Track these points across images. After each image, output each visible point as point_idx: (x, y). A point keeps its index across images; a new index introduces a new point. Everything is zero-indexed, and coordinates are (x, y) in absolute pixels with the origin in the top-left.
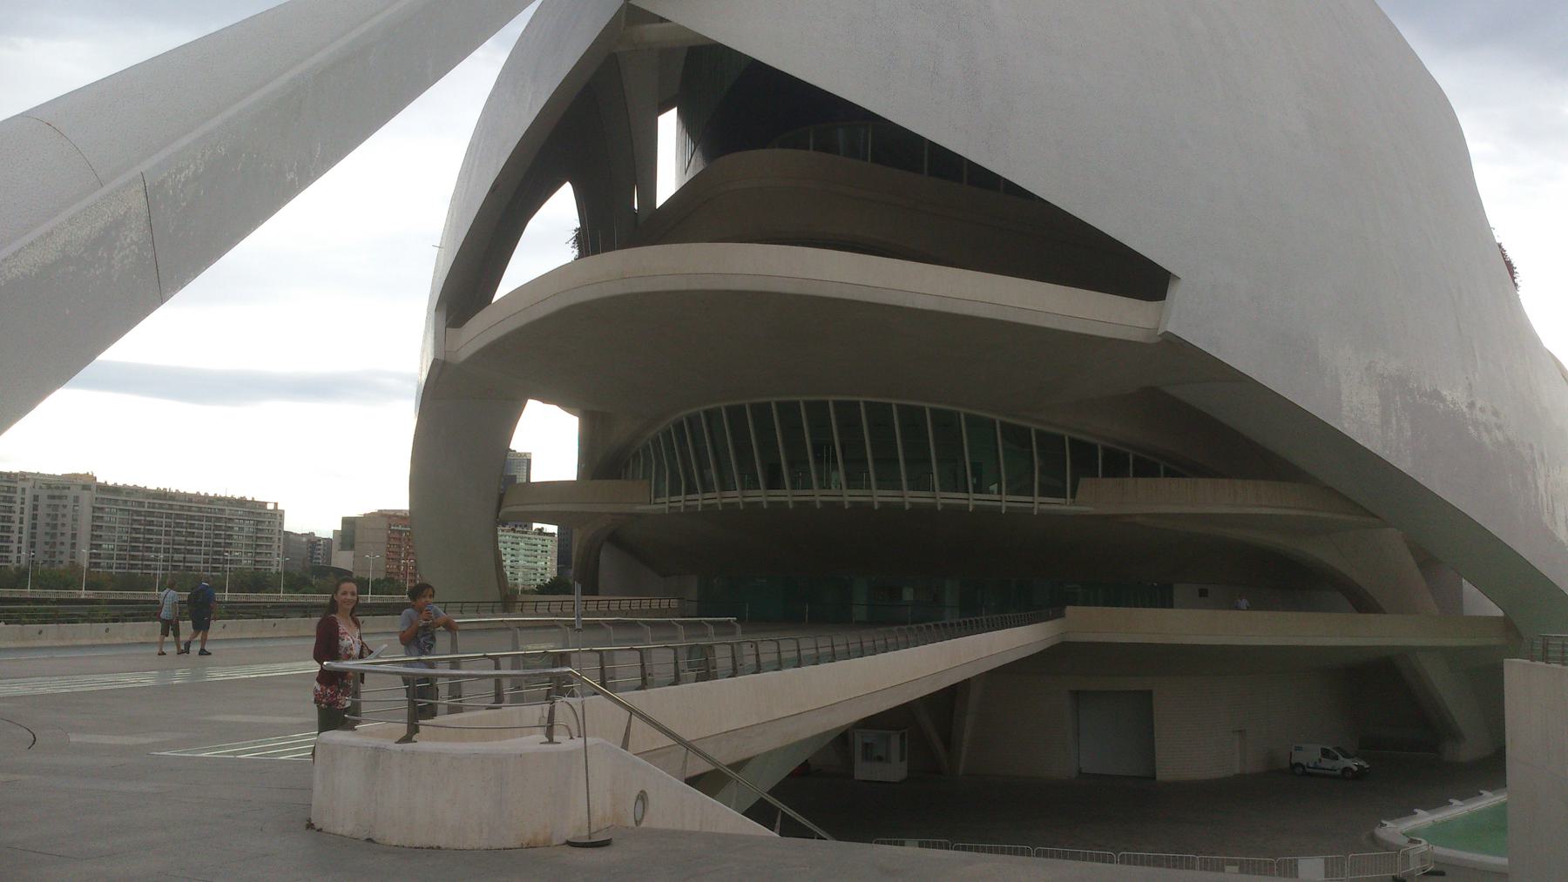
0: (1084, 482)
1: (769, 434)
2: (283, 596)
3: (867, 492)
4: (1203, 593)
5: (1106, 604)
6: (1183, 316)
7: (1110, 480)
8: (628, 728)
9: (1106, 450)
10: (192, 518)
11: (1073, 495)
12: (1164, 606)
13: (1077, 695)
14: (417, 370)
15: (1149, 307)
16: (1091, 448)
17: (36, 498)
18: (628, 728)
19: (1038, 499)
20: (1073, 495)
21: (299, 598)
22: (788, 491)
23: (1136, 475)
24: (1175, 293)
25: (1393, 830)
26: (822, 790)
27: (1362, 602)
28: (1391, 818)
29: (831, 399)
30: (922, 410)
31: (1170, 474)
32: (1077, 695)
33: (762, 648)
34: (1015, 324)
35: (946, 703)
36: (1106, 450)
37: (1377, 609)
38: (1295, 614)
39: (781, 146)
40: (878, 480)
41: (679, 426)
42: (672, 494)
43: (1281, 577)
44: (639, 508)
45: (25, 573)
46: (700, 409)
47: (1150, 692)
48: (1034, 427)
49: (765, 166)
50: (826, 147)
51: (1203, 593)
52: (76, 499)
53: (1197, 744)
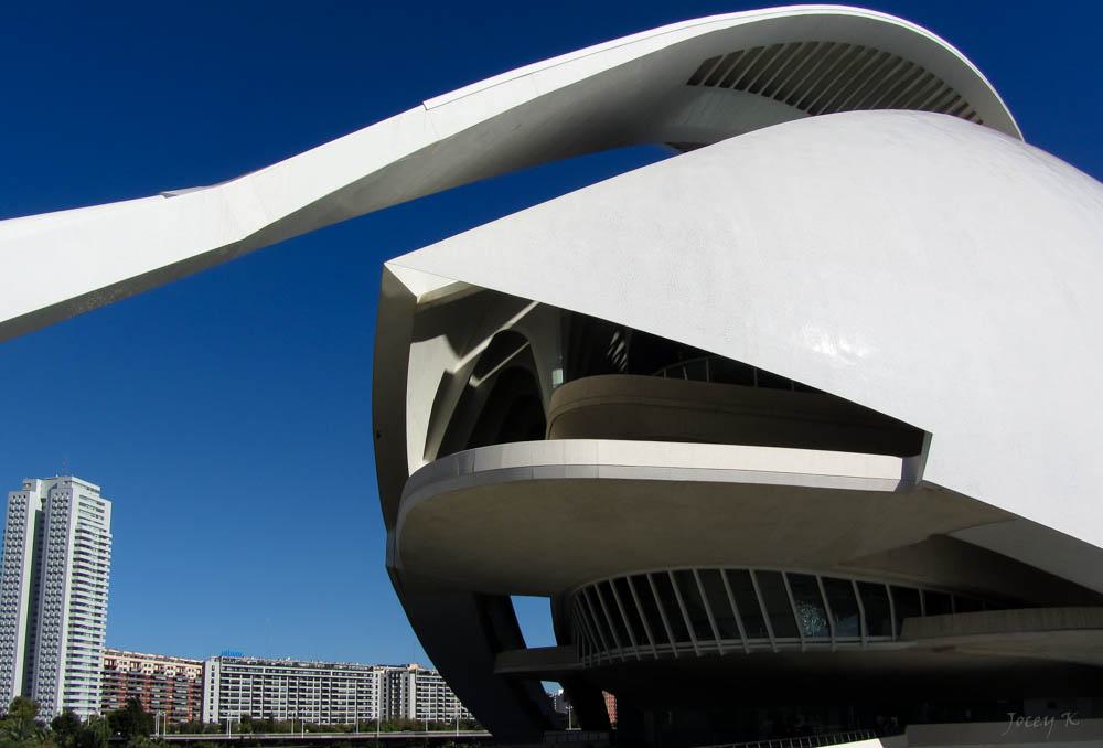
0: (909, 622)
3: (764, 640)
7: (930, 618)
9: (928, 594)
11: (899, 633)
16: (914, 592)
22: (744, 639)
23: (959, 610)
30: (849, 583)
48: (854, 579)
51: (1052, 706)
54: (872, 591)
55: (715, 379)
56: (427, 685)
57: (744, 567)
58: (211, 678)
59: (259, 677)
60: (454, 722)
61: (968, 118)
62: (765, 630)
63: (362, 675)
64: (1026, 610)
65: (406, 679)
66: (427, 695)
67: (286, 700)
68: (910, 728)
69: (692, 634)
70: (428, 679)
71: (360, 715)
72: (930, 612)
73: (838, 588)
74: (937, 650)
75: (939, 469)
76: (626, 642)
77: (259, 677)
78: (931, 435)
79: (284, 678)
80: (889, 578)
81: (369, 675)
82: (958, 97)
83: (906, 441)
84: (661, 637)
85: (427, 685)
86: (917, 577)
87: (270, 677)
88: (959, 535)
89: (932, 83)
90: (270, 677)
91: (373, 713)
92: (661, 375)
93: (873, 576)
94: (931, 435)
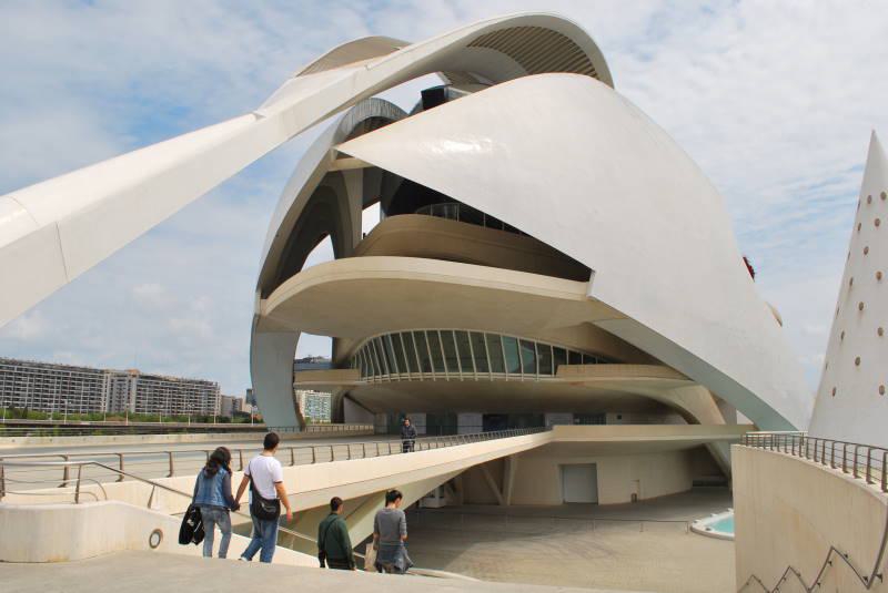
1: (403, 347)
2: (215, 425)
4: (619, 417)
6: (598, 288)
8: (314, 124)
9: (571, 353)
13: (563, 467)
15: (583, 284)
16: (563, 351)
17: (112, 381)
18: (314, 124)
19: (539, 375)
22: (433, 373)
23: (585, 363)
24: (595, 279)
25: (701, 524)
27: (690, 420)
29: (469, 330)
30: (466, 333)
31: (601, 362)
32: (563, 467)
35: (500, 465)
36: (585, 356)
37: (699, 423)
40: (463, 367)
41: (370, 343)
43: (653, 410)
46: (380, 335)
47: (594, 465)
48: (536, 341)
49: (409, 222)
50: (440, 214)
51: (619, 417)
53: (614, 488)
55: (462, 219)
57: (479, 331)
59: (11, 374)
61: (594, 76)
64: (612, 365)
66: (79, 398)
67: (59, 395)
69: (475, 369)
72: (571, 363)
75: (600, 288)
76: (403, 370)
77: (11, 374)
78: (424, 93)
79: (31, 376)
82: (590, 65)
84: (403, 370)
86: (569, 343)
87: (20, 374)
88: (602, 325)
90: (20, 374)
92: (427, 213)
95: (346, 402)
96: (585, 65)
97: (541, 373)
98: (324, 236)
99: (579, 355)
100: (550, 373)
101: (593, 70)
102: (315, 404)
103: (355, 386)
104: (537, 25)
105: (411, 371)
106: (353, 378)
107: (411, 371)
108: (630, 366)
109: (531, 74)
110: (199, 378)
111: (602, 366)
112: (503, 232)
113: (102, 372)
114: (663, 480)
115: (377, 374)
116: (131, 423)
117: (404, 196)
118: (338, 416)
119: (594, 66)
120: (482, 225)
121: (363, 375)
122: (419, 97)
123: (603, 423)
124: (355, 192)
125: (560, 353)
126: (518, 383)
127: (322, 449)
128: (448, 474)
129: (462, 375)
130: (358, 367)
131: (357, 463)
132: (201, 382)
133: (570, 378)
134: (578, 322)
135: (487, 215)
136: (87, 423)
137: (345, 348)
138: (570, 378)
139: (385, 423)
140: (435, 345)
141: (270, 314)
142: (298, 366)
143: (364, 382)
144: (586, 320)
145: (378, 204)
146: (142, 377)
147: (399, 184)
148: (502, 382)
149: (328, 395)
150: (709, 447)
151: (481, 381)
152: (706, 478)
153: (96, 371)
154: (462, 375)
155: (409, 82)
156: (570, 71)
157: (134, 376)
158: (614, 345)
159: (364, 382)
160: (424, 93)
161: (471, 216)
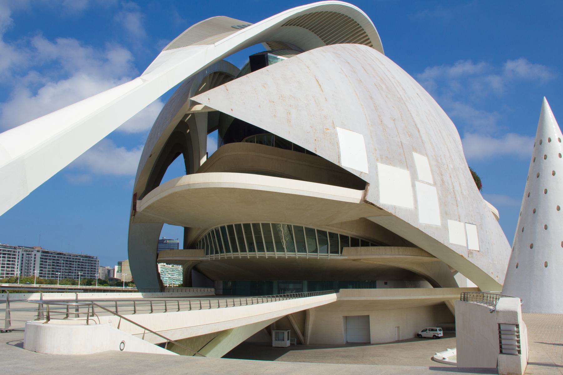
0: (345, 249)
3: (305, 253)
5: (353, 288)
7: (353, 248)
9: (352, 238)
10: (71, 261)
11: (341, 253)
12: (371, 288)
14: (451, 241)
16: (347, 237)
17: (23, 255)
20: (341, 253)
21: (102, 287)
22: (232, 253)
23: (362, 246)
26: (260, 345)
28: (439, 352)
31: (373, 245)
33: (220, 301)
34: (245, 189)
35: (304, 314)
36: (362, 240)
38: (414, 289)
39: (247, 141)
40: (277, 249)
42: (211, 254)
43: (406, 278)
44: (201, 259)
45: (17, 278)
48: (328, 231)
49: (238, 148)
51: (386, 283)
52: (35, 255)
54: (332, 235)
55: (294, 150)
56: (46, 259)
57: (301, 225)
58: (36, 257)
60: (17, 278)
62: (305, 248)
63: (55, 257)
64: (381, 247)
65: (35, 255)
68: (341, 290)
70: (47, 256)
71: (7, 274)
73: (322, 234)
74: (354, 260)
78: (251, 57)
80: (339, 231)
81: (14, 252)
83: (357, 183)
85: (46, 259)
86: (349, 233)
88: (369, 218)
89: (367, 38)
91: (15, 273)
93: (335, 230)
94: (368, 183)
95: (193, 271)
96: (365, 39)
97: (331, 253)
98: (177, 155)
99: (358, 240)
100: (337, 252)
101: (370, 42)
102: (171, 274)
103: (201, 261)
104: (329, 10)
105: (233, 252)
106: (198, 256)
107: (233, 252)
108: (393, 247)
109: (327, 44)
110: (84, 254)
111: (373, 247)
112: (305, 154)
113: (15, 248)
114: (422, 321)
115: (217, 252)
116: (38, 286)
117: (234, 131)
118: (188, 282)
119: (369, 36)
120: (291, 149)
121: (207, 254)
122: (248, 61)
123: (374, 287)
124: (202, 125)
125: (344, 239)
126: (316, 259)
127: (172, 304)
128: (275, 318)
129: (240, 254)
130: (203, 248)
131: (195, 313)
132: (86, 257)
133: (350, 257)
134: (357, 218)
135: (294, 144)
136: (7, 285)
137: (193, 236)
138: (350, 257)
139: (221, 287)
140: (257, 232)
141: (143, 211)
142: (161, 246)
143: (208, 258)
144: (365, 216)
145: (217, 130)
146: (43, 252)
147: (232, 120)
148: (304, 259)
149: (180, 268)
150: (447, 303)
151: (270, 258)
152: (442, 321)
153: (11, 247)
154: (240, 254)
155: (429, 166)
156: (349, 42)
157: (38, 251)
158: (380, 232)
159: (208, 258)
160: (251, 58)
161: (282, 144)
